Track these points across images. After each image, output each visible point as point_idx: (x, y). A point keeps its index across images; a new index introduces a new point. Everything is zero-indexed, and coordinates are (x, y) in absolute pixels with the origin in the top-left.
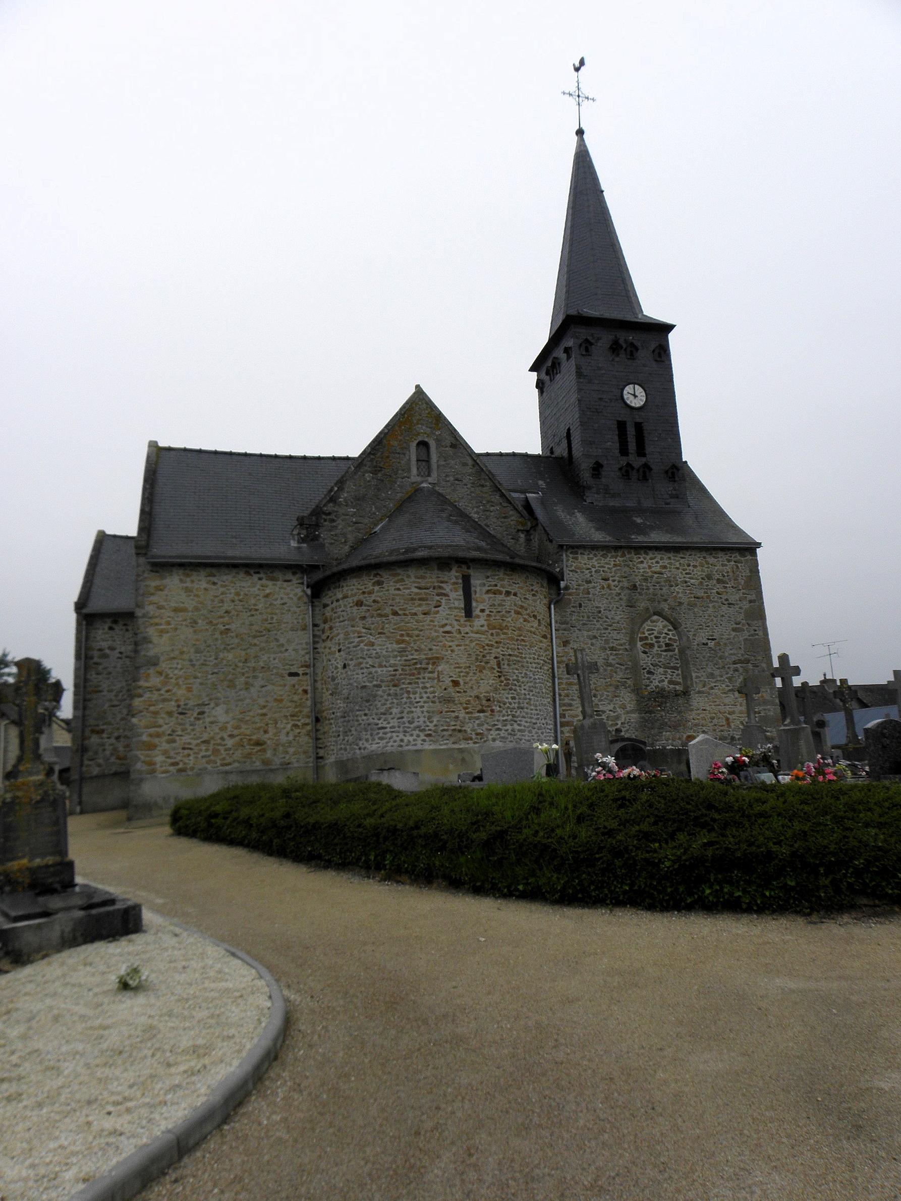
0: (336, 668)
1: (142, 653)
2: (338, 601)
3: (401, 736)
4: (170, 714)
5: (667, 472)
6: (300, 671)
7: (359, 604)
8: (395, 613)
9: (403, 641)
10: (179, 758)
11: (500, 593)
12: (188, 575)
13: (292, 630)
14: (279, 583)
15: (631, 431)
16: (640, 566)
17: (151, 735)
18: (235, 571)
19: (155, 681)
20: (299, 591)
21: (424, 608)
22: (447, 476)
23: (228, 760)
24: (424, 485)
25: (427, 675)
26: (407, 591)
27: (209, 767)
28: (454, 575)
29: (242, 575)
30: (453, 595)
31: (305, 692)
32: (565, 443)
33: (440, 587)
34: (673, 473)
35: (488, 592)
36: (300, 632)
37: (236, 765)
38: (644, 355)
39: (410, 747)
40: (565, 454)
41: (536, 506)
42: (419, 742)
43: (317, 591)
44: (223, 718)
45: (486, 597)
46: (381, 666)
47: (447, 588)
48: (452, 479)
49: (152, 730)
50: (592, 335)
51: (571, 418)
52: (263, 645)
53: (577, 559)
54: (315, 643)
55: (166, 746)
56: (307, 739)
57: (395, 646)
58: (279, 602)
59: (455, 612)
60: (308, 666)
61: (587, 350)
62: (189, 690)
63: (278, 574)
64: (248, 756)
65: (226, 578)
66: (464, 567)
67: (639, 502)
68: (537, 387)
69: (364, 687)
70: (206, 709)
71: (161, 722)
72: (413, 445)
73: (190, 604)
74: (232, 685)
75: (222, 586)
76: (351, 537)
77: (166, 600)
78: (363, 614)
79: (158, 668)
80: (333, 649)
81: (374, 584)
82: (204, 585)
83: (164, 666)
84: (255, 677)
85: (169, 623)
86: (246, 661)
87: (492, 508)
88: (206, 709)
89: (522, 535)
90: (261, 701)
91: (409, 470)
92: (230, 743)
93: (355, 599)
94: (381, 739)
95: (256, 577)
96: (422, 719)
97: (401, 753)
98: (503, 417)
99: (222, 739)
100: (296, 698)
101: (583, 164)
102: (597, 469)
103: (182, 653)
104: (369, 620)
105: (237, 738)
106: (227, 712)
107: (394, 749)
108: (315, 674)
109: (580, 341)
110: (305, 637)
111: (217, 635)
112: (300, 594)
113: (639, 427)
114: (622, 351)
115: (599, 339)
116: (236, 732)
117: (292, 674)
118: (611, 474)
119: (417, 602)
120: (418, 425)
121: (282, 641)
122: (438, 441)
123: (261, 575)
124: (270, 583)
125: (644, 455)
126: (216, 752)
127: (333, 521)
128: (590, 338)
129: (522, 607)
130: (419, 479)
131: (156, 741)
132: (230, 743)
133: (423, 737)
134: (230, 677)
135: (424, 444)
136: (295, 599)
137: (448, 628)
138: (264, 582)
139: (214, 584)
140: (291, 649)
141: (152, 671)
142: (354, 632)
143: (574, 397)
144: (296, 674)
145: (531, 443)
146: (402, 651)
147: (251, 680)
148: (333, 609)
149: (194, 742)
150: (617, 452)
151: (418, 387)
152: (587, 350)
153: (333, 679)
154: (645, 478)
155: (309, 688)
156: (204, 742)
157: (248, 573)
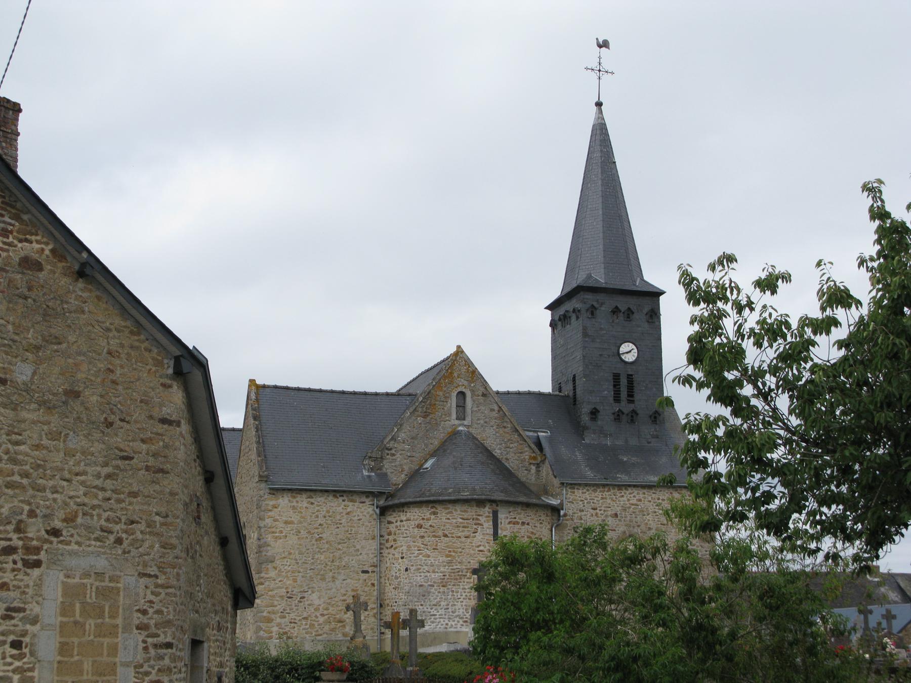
0: (399, 570)
1: (264, 553)
2: (401, 521)
3: (447, 621)
4: (282, 597)
5: (650, 417)
6: (370, 570)
7: (420, 526)
8: (445, 536)
9: (450, 556)
10: (287, 629)
11: (518, 523)
12: (294, 497)
13: (365, 539)
14: (357, 504)
15: (624, 381)
16: (621, 499)
17: (269, 612)
18: (326, 494)
19: (272, 574)
20: (370, 510)
21: (466, 533)
22: (478, 419)
23: (320, 632)
24: (461, 428)
25: (466, 580)
26: (454, 521)
27: (307, 636)
28: (487, 510)
29: (331, 498)
30: (486, 525)
31: (373, 585)
32: (570, 386)
33: (477, 519)
34: (655, 417)
35: (510, 523)
36: (371, 541)
37: (325, 635)
38: (640, 318)
39: (452, 629)
40: (571, 394)
41: (545, 444)
42: (459, 626)
43: (384, 511)
44: (317, 602)
45: (508, 526)
46: (434, 572)
47: (482, 520)
48: (482, 422)
49: (270, 609)
50: (597, 301)
51: (577, 368)
52: (345, 549)
53: (574, 493)
54: (381, 549)
55: (278, 620)
56: (373, 619)
57: (445, 559)
58: (356, 518)
59: (487, 537)
60: (376, 566)
61: (592, 313)
62: (295, 581)
63: (355, 497)
64: (333, 630)
65: (320, 499)
66: (494, 505)
67: (626, 441)
68: (551, 325)
69: (421, 586)
70: (305, 595)
71: (276, 603)
72: (454, 394)
73: (295, 518)
74: (323, 579)
75: (318, 506)
76: (406, 468)
77: (279, 515)
78: (422, 534)
79: (274, 565)
80: (396, 556)
81: (430, 514)
82: (305, 505)
83: (278, 563)
84: (339, 573)
85: (281, 532)
86: (333, 561)
87: (511, 445)
88: (305, 595)
89: (533, 468)
90: (343, 591)
91: (450, 415)
92: (321, 619)
93: (417, 523)
94: (433, 622)
95: (341, 499)
96: (461, 611)
97: (446, 633)
98: (520, 356)
99: (316, 617)
100: (367, 589)
101: (600, 139)
102: (594, 413)
103: (290, 554)
104: (427, 539)
105: (326, 617)
106: (319, 598)
107: (441, 630)
108: (380, 572)
109: (588, 306)
110: (374, 545)
111: (314, 542)
112: (371, 512)
113: (630, 378)
114: (621, 314)
115: (602, 304)
116: (325, 612)
117: (364, 572)
118: (606, 417)
119: (461, 529)
120: (456, 371)
121: (358, 547)
122: (472, 391)
123: (345, 498)
124: (351, 504)
125: (632, 402)
126: (312, 626)
127: (393, 455)
128: (595, 304)
129: (532, 533)
130: (457, 422)
131: (273, 616)
132: (321, 619)
133: (461, 622)
134: (322, 572)
135: (462, 394)
136: (368, 516)
137: (481, 548)
138: (346, 503)
139: (312, 503)
140: (364, 553)
141: (270, 566)
142: (415, 546)
143: (579, 355)
144: (367, 572)
145: (546, 386)
146: (450, 562)
147: (336, 575)
148: (397, 527)
149: (298, 618)
150: (611, 399)
151: (459, 347)
152: (592, 313)
153: (397, 578)
154: (633, 421)
155: (376, 582)
156: (304, 618)
157: (335, 496)
